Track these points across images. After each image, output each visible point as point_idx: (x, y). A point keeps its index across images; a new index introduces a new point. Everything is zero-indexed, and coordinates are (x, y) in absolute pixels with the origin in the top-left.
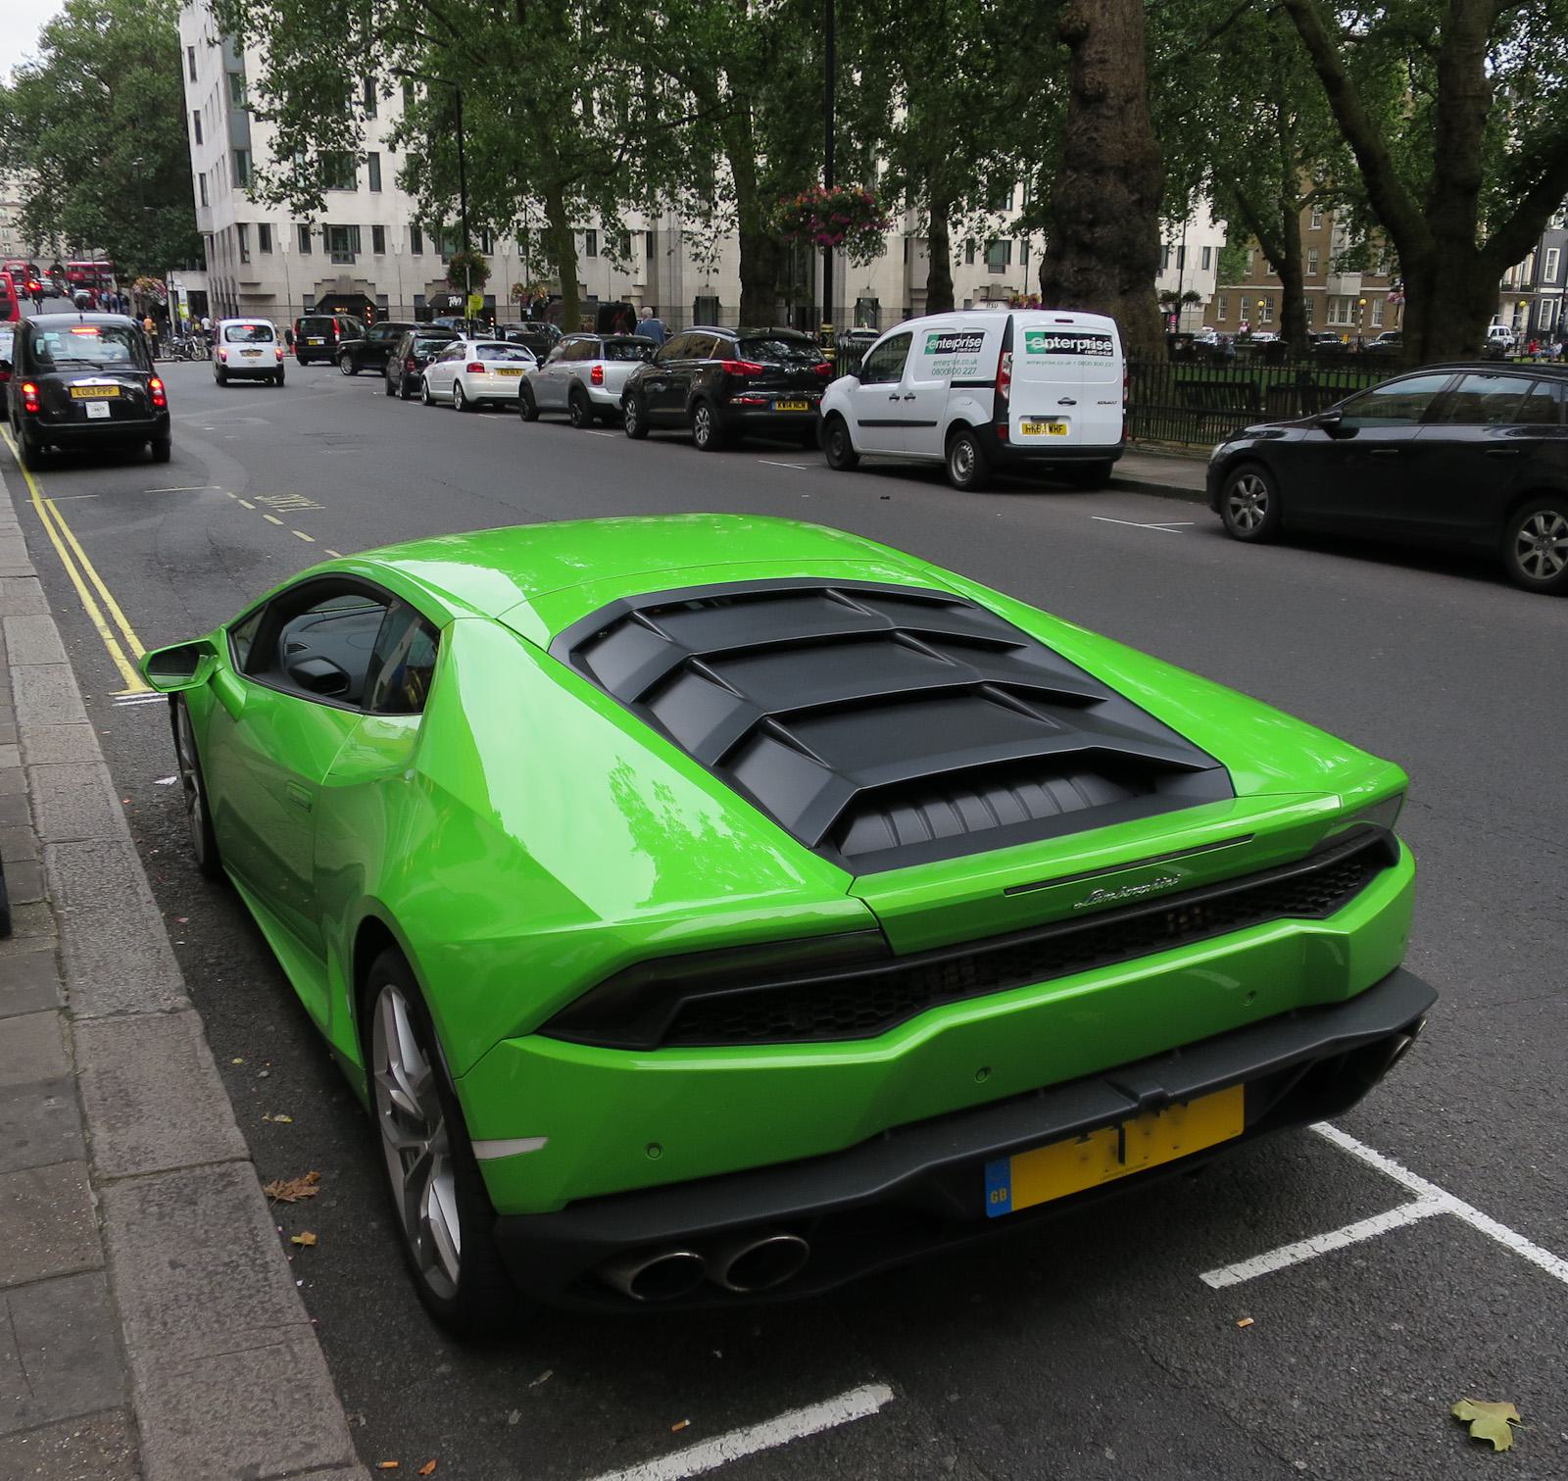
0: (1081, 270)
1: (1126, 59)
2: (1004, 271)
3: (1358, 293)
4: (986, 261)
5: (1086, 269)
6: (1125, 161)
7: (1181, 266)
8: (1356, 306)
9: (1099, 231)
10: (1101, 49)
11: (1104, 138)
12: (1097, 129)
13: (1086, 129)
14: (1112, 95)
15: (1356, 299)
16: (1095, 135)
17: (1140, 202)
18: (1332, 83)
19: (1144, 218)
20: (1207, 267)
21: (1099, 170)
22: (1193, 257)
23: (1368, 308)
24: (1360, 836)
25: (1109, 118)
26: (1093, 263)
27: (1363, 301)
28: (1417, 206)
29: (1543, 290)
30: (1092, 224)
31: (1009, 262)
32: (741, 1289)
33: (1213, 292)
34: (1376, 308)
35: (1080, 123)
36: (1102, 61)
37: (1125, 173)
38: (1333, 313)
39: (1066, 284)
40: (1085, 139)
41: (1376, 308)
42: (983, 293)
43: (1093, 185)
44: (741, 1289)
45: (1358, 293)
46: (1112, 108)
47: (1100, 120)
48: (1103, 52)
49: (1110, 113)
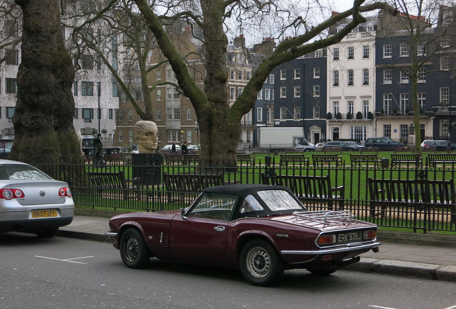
0: (33, 118)
1: (49, 13)
2: (90, 121)
3: (180, 128)
4: (83, 117)
5: (35, 117)
6: (53, 63)
7: (99, 118)
8: (180, 134)
9: (41, 98)
10: (36, 8)
11: (41, 51)
12: (37, 47)
13: (32, 47)
14: (44, 30)
15: (179, 131)
16: (36, 50)
17: (62, 83)
18: (158, 34)
19: (65, 91)
20: (111, 118)
21: (40, 67)
22: (105, 113)
23: (185, 134)
24: (304, 98)
25: (43, 41)
26: (40, 114)
27: (182, 131)
28: (201, 84)
29: (258, 125)
30: (38, 94)
31: (93, 118)
32: (241, 234)
33: (115, 129)
34: (189, 134)
35: (28, 44)
36: (38, 14)
37: (54, 71)
38: (170, 137)
39: (25, 125)
40: (31, 52)
41: (189, 134)
42: (7, 131)
43: (37, 75)
44: (241, 234)
45: (180, 128)
46: (44, 37)
47: (39, 43)
48: (38, 9)
49: (43, 39)
